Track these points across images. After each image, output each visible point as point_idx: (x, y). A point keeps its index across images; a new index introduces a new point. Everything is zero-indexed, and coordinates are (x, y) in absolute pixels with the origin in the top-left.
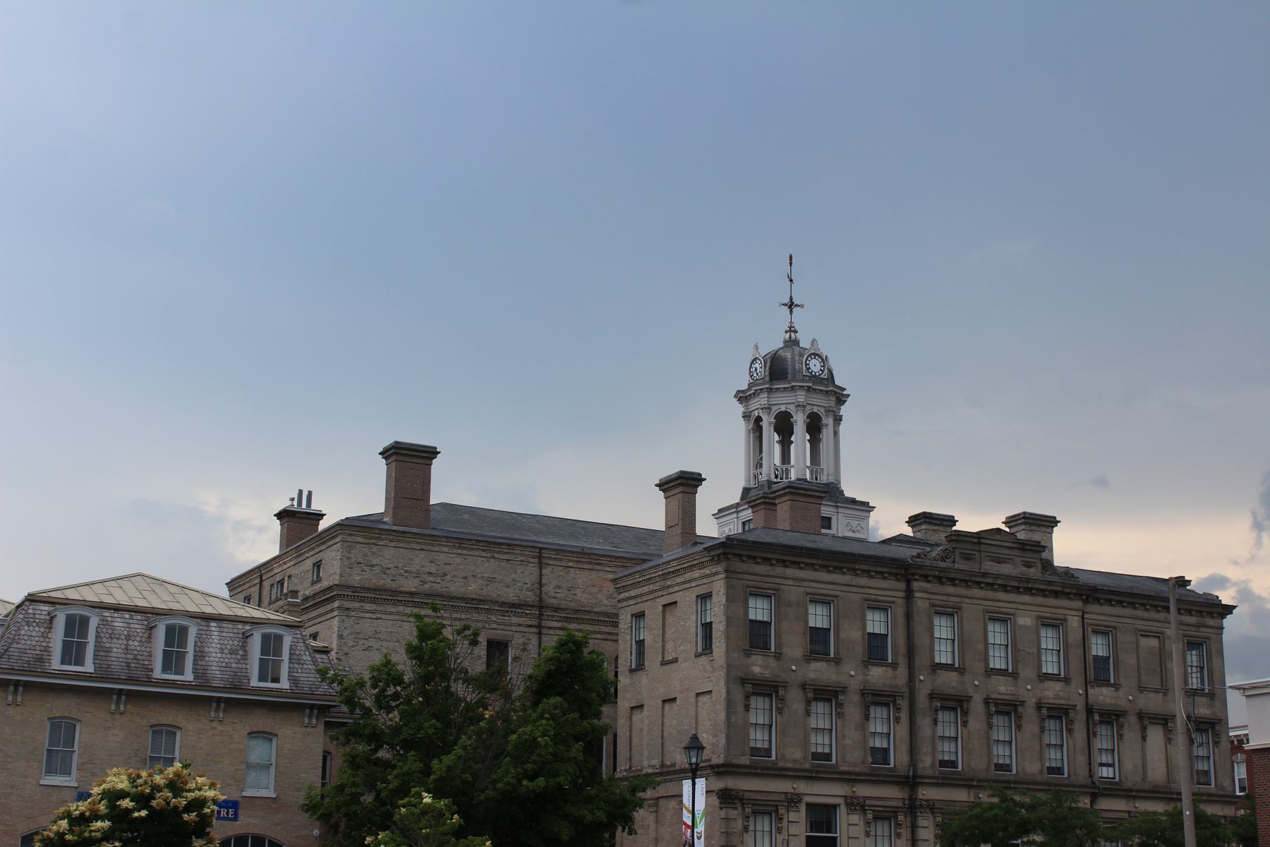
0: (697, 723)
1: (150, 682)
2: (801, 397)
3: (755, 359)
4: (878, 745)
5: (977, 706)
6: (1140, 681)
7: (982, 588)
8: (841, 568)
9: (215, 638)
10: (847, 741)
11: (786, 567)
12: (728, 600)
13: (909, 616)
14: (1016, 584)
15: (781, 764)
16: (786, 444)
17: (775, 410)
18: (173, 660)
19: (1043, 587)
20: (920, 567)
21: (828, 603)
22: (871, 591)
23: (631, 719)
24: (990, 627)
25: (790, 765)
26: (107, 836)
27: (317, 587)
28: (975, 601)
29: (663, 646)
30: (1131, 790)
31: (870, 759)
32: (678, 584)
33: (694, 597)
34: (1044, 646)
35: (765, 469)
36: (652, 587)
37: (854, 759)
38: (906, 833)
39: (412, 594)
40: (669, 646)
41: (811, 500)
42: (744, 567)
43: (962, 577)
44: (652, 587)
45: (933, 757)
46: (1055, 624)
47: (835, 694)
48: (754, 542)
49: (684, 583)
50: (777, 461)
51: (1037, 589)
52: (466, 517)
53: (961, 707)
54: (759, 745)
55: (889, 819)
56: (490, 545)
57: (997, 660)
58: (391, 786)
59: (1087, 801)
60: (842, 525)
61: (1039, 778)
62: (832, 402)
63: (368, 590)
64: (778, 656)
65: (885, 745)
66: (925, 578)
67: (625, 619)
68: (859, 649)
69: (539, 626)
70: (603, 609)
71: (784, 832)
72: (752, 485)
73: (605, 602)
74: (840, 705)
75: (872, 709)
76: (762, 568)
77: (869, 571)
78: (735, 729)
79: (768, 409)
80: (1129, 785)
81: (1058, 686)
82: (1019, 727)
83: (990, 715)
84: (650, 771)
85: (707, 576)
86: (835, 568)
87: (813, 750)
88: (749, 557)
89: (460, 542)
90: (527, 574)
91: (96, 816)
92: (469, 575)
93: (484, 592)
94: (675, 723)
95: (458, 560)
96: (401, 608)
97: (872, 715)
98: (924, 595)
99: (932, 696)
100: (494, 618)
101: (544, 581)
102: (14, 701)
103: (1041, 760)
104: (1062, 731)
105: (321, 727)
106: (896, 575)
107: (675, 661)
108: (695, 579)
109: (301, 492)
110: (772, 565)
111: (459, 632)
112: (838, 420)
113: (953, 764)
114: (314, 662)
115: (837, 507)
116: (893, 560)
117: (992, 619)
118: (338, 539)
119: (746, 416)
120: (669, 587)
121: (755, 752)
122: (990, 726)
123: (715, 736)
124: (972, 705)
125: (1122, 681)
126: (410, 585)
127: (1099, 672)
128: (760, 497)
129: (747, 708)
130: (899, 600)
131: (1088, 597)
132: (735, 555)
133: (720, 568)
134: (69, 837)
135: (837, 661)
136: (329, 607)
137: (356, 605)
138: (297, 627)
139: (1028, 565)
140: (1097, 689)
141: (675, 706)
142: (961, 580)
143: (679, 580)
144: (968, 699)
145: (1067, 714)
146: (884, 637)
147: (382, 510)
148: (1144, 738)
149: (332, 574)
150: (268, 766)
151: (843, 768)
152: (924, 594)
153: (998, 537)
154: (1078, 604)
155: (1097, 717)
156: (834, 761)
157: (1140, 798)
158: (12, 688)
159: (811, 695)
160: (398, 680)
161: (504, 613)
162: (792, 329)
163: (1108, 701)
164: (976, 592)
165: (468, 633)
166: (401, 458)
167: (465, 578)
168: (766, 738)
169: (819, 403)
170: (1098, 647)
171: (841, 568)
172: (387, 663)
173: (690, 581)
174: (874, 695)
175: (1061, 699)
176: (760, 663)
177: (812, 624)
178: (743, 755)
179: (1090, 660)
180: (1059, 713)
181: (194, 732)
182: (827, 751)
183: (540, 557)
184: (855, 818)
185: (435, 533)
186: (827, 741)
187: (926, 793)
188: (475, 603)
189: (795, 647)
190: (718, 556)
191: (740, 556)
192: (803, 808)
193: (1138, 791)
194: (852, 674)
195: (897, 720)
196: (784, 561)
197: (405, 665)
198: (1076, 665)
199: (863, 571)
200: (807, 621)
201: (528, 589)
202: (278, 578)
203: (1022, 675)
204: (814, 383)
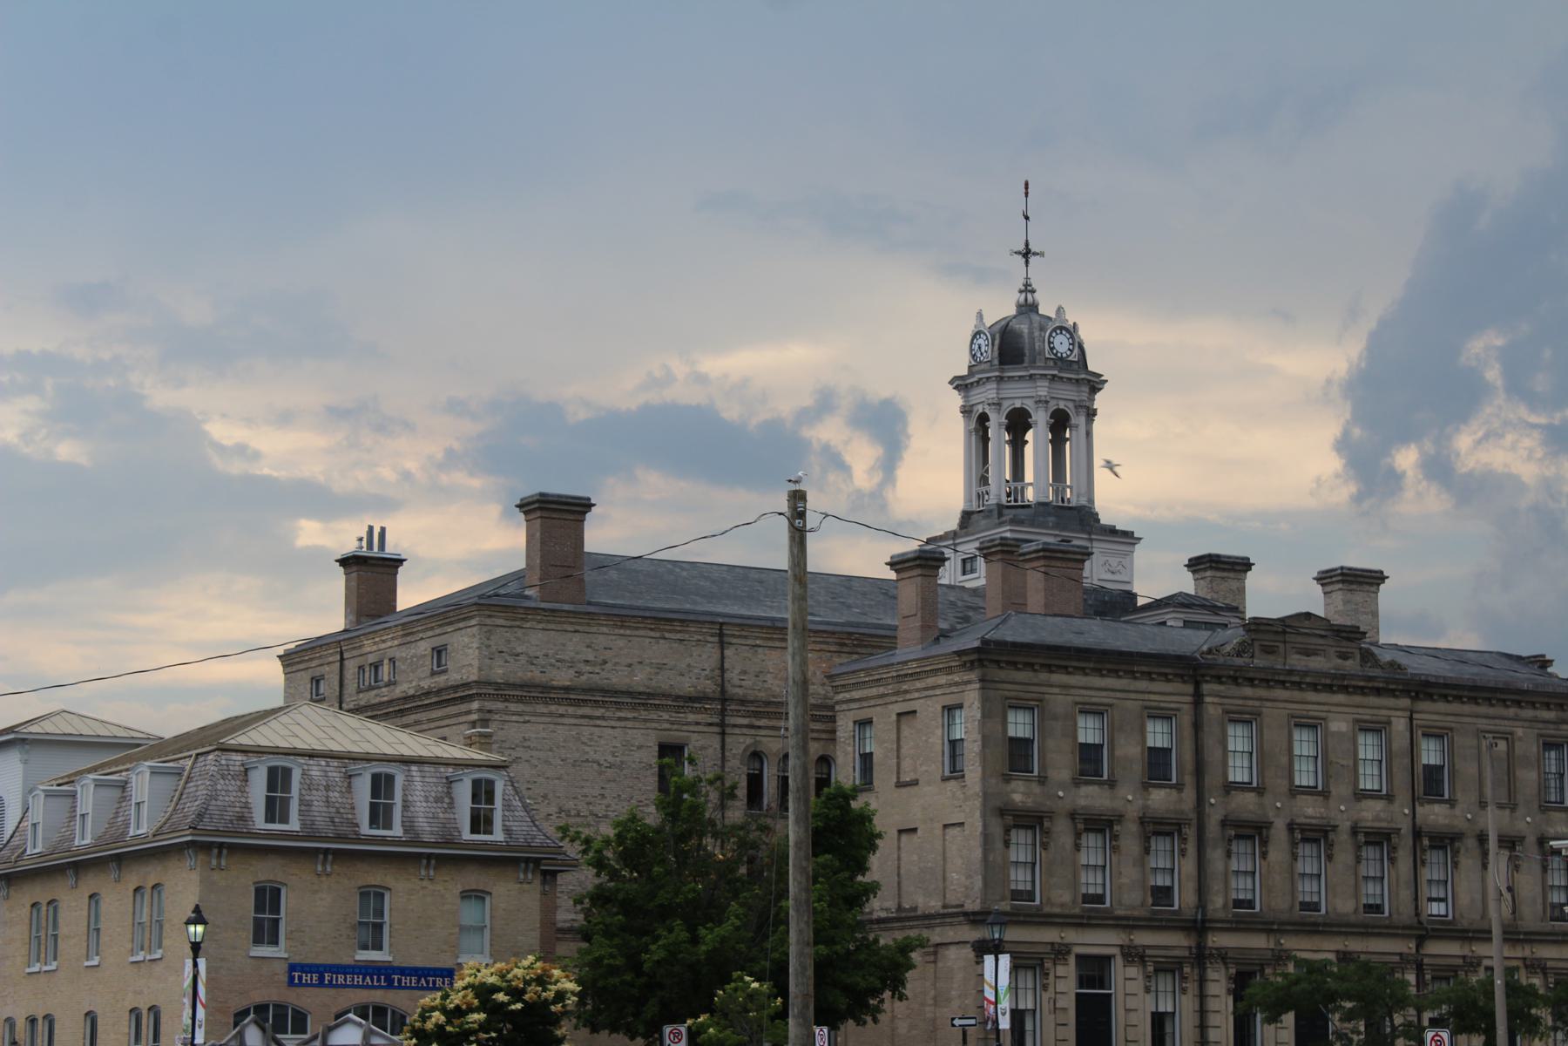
0: (944, 859)
1: (359, 840)
2: (1042, 389)
3: (979, 333)
4: (1160, 883)
5: (1279, 833)
9: (418, 785)
10: (1125, 880)
11: (1051, 672)
12: (983, 716)
13: (1197, 726)
14: (1328, 681)
15: (1047, 909)
16: (1018, 445)
17: (1007, 406)
18: (379, 815)
20: (1210, 666)
22: (1153, 697)
24: (1296, 735)
25: (1057, 910)
26: (484, 1027)
27: (441, 680)
28: (1278, 704)
30: (1467, 931)
31: (1150, 901)
32: (917, 690)
34: (1362, 756)
36: (882, 690)
37: (1132, 900)
38: (1192, 987)
39: (567, 689)
40: (906, 764)
41: (1070, 565)
42: (1002, 674)
43: (1262, 676)
44: (882, 690)
45: (1226, 896)
46: (1376, 728)
47: (1110, 824)
51: (1355, 687)
53: (1260, 834)
54: (1021, 887)
55: (1173, 972)
56: (659, 622)
57: (1304, 775)
58: (656, 958)
59: (1413, 945)
61: (1353, 919)
63: (514, 686)
65: (1168, 883)
66: (1218, 679)
67: (845, 726)
68: (1138, 769)
69: (722, 725)
71: (1051, 989)
72: (974, 508)
74: (1115, 837)
77: (1150, 673)
78: (993, 871)
80: (1465, 924)
81: (1378, 805)
82: (1330, 858)
83: (1294, 844)
84: (883, 915)
85: (956, 684)
86: (1109, 671)
88: (1008, 663)
89: (623, 618)
90: (706, 657)
91: (471, 1010)
92: (635, 660)
93: (654, 683)
94: (915, 858)
95: (621, 643)
96: (553, 708)
98: (1216, 700)
99: (1224, 823)
100: (666, 716)
101: (726, 665)
102: (219, 864)
103: (1357, 896)
104: (1382, 860)
107: (915, 783)
109: (371, 528)
112: (1091, 414)
113: (1250, 904)
116: (1179, 658)
117: (1299, 725)
118: (473, 622)
119: (966, 411)
120: (906, 692)
121: (1016, 895)
122: (1295, 857)
123: (969, 877)
124: (1273, 831)
125: (1459, 796)
126: (563, 677)
127: (1431, 783)
129: (1007, 844)
130: (1186, 707)
133: (973, 676)
134: (449, 1029)
135: (1112, 784)
136: (463, 707)
137: (500, 705)
138: (504, 767)
139: (1344, 656)
140: (1427, 807)
141: (915, 838)
142: (1262, 680)
143: (918, 685)
144: (1268, 825)
146: (1166, 752)
148: (1485, 866)
150: (482, 929)
151: (1120, 912)
152: (1215, 698)
154: (1405, 702)
155: (1426, 842)
156: (1108, 904)
157: (1478, 939)
158: (215, 851)
159: (1081, 826)
161: (678, 709)
162: (1027, 288)
163: (1442, 821)
164: (1280, 693)
166: (546, 514)
167: (630, 665)
168: (1029, 878)
169: (1066, 397)
170: (1430, 754)
171: (1116, 671)
173: (933, 688)
177: (1081, 739)
178: (1003, 899)
179: (1419, 770)
180: (1380, 838)
181: (407, 896)
182: (1100, 891)
183: (721, 635)
184: (1133, 971)
185: (591, 609)
187: (1217, 940)
189: (1062, 767)
190: (972, 662)
191: (998, 662)
192: (1072, 960)
193: (1474, 931)
194: (1129, 799)
195: (1183, 853)
197: (652, 817)
198: (1401, 778)
200: (1075, 737)
202: (372, 659)
203: (1334, 792)
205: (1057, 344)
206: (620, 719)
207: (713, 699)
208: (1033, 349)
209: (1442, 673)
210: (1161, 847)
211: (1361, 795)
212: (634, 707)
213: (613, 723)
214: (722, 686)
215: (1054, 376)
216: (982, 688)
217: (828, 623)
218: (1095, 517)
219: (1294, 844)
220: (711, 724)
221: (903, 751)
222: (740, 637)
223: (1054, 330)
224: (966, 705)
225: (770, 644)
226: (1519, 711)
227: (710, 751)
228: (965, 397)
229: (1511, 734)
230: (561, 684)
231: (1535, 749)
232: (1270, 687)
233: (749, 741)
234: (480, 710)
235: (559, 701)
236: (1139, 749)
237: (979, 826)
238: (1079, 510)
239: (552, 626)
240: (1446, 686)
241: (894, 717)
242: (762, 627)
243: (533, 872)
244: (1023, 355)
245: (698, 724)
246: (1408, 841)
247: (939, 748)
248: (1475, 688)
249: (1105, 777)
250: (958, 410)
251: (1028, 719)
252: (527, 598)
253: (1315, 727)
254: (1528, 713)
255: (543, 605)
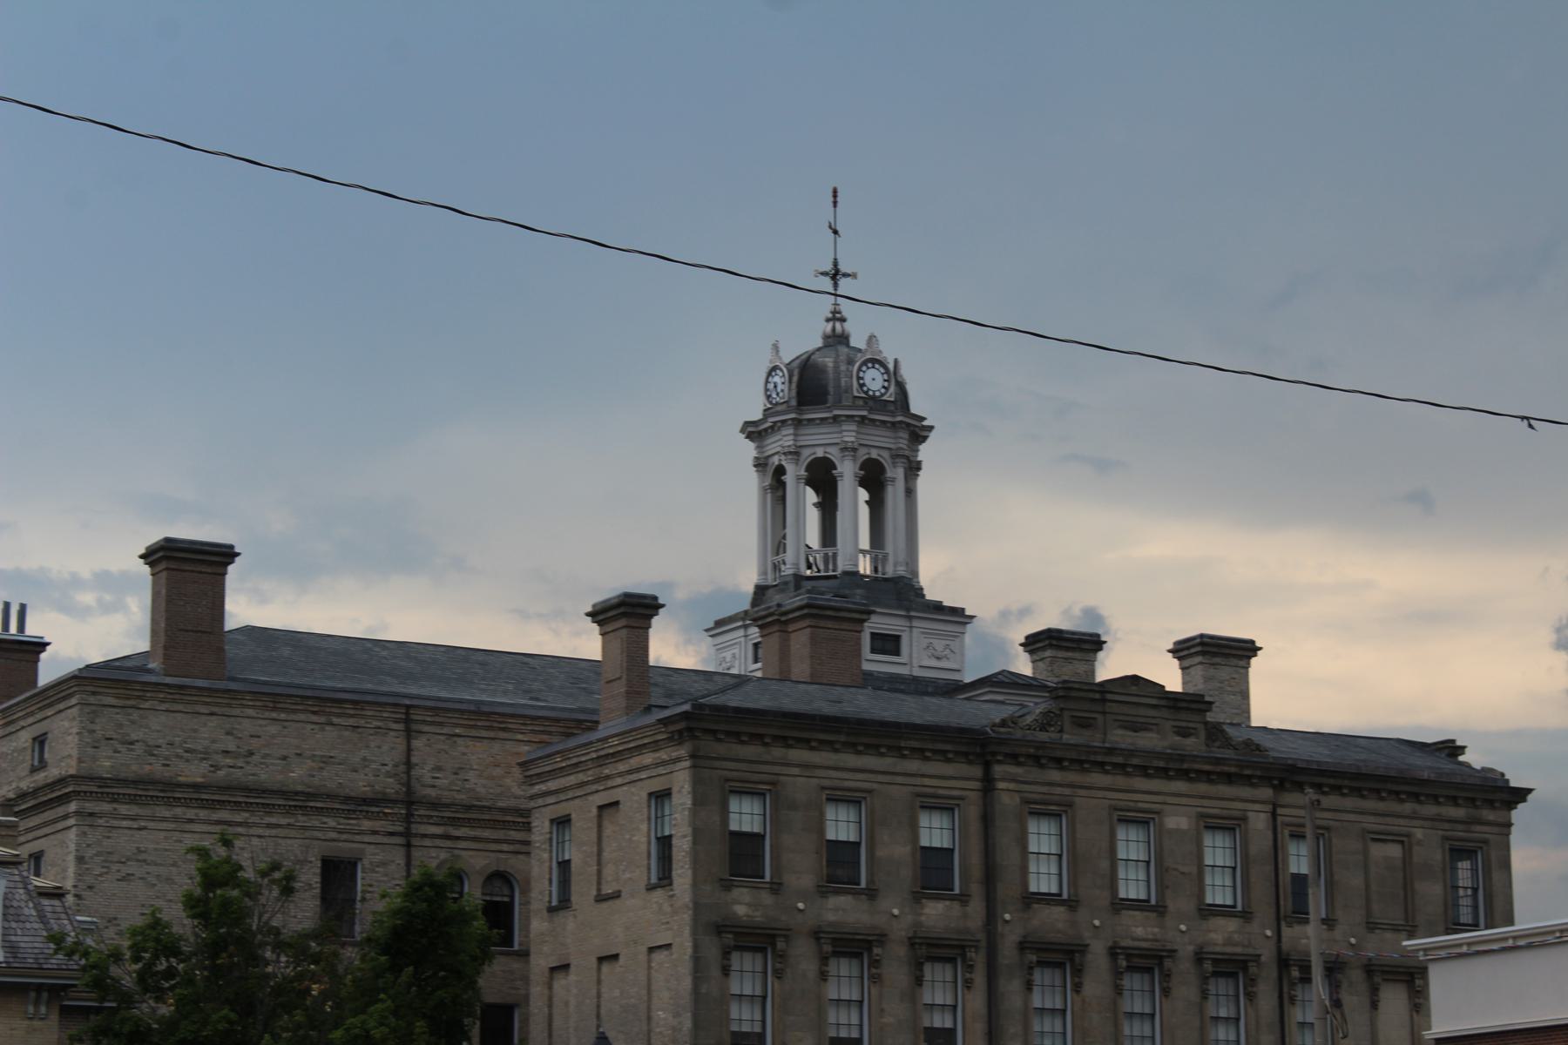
2: (849, 434)
3: (774, 369)
4: (937, 1024)
6: (1369, 913)
7: (1107, 772)
8: (877, 747)
10: (888, 1020)
11: (789, 747)
12: (694, 804)
13: (987, 819)
14: (1162, 764)
16: (828, 507)
17: (807, 455)
19: (1207, 767)
21: (857, 803)
22: (927, 781)
23: (550, 988)
24: (1121, 833)
27: (41, 778)
29: (599, 872)
32: (620, 774)
33: (644, 795)
35: (789, 556)
36: (582, 777)
39: (196, 787)
40: (608, 871)
41: (845, 626)
42: (721, 749)
43: (1074, 755)
44: (582, 777)
46: (1230, 825)
47: (868, 945)
48: (737, 710)
49: (630, 772)
50: (813, 537)
51: (1198, 772)
52: (286, 651)
53: (1072, 961)
54: (746, 1028)
56: (325, 704)
57: (1132, 885)
60: (919, 654)
62: (903, 441)
63: (124, 782)
64: (776, 888)
65: (948, 1024)
66: (1014, 758)
67: (541, 826)
69: (407, 834)
70: (512, 803)
72: (770, 582)
73: (517, 791)
74: (875, 963)
75: (927, 968)
76: (751, 751)
77: (922, 750)
79: (795, 454)
81: (1232, 925)
82: (1166, 992)
85: (664, 763)
86: (867, 746)
87: (833, 1034)
88: (728, 733)
89: (276, 700)
92: (291, 752)
94: (617, 993)
95: (273, 729)
96: (179, 811)
97: (928, 976)
98: (1012, 786)
99: (1023, 946)
100: (332, 823)
101: (414, 760)
104: (1237, 996)
105: (55, 1017)
106: (966, 754)
107: (617, 895)
108: (646, 768)
109: (7, 606)
110: (766, 744)
111: (264, 874)
112: (914, 468)
114: (42, 917)
115: (910, 618)
116: (962, 731)
118: (74, 701)
119: (760, 464)
120: (608, 777)
122: (1118, 990)
123: (677, 1015)
124: (1089, 957)
126: (194, 772)
128: (769, 613)
129: (726, 971)
131: (1282, 782)
132: (706, 731)
133: (683, 751)
135: (871, 894)
136: (60, 811)
137: (106, 807)
139: (1184, 733)
141: (618, 967)
142: (1072, 761)
143: (622, 767)
144: (1083, 949)
145: (1245, 969)
147: (143, 645)
148: (1374, 1005)
149: (65, 756)
152: (1011, 783)
153: (1134, 689)
154: (1266, 793)
159: (828, 948)
160: (171, 948)
162: (836, 317)
165: (277, 875)
167: (284, 758)
168: (758, 1016)
169: (880, 444)
172: (156, 924)
173: (638, 770)
174: (930, 945)
175: (1236, 945)
176: (747, 899)
177: (831, 835)
179: (1285, 881)
180: (1231, 968)
182: (855, 1035)
183: (407, 721)
185: (233, 686)
186: (855, 1020)
188: (300, 801)
189: (803, 873)
190: (680, 732)
191: (714, 732)
194: (894, 913)
195: (968, 984)
196: (785, 738)
197: (181, 923)
199: (913, 750)
200: (821, 831)
201: (388, 775)
204: (871, 410)
205: (868, 381)
206: (269, 826)
207: (395, 802)
208: (838, 386)
209: (1317, 758)
210: (938, 977)
211: (1209, 911)
212: (288, 811)
213: (260, 831)
214: (408, 785)
215: (863, 417)
216: (693, 766)
217: (553, 709)
218: (919, 592)
219: (1117, 974)
220: (392, 834)
221: (605, 854)
222: (432, 723)
223: (865, 363)
224: (675, 790)
225: (474, 733)
226: (1417, 807)
227: (393, 867)
228: (760, 448)
229: (1408, 835)
230: (190, 780)
231: (1439, 857)
232: (1084, 770)
233: (443, 855)
234: (77, 813)
235: (187, 803)
236: (908, 849)
237: (689, 945)
238: (896, 581)
239: (180, 707)
240: (1322, 773)
241: (595, 811)
242: (462, 712)
243: (48, 1004)
244: (826, 393)
245: (375, 833)
246: (1272, 972)
247: (644, 847)
248: (1359, 776)
249: (863, 884)
250: (750, 462)
251: (757, 809)
252: (150, 671)
253: (1145, 823)
254: (1430, 810)
255: (168, 680)
